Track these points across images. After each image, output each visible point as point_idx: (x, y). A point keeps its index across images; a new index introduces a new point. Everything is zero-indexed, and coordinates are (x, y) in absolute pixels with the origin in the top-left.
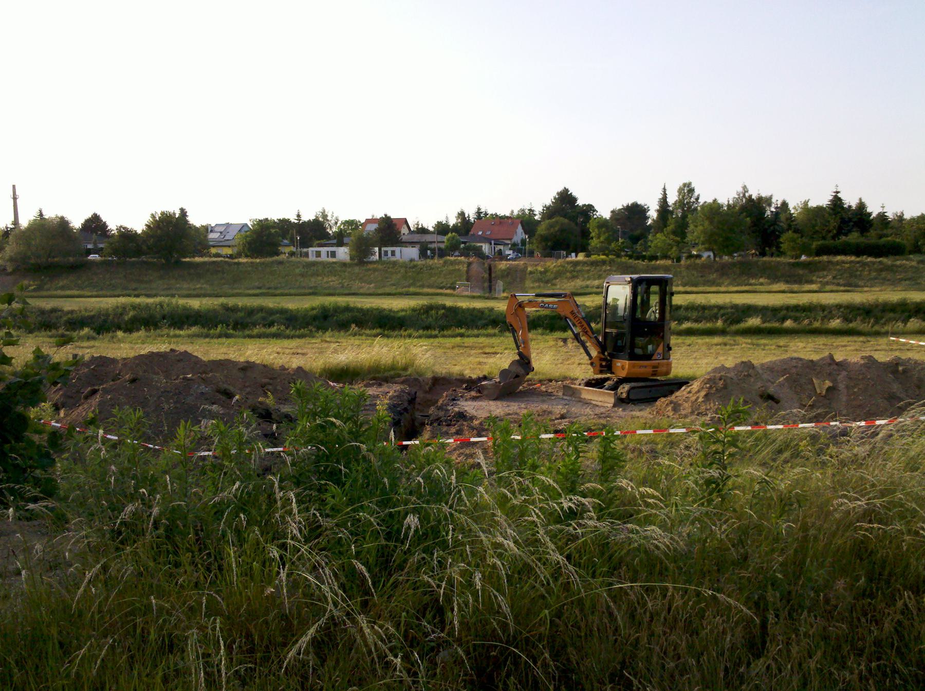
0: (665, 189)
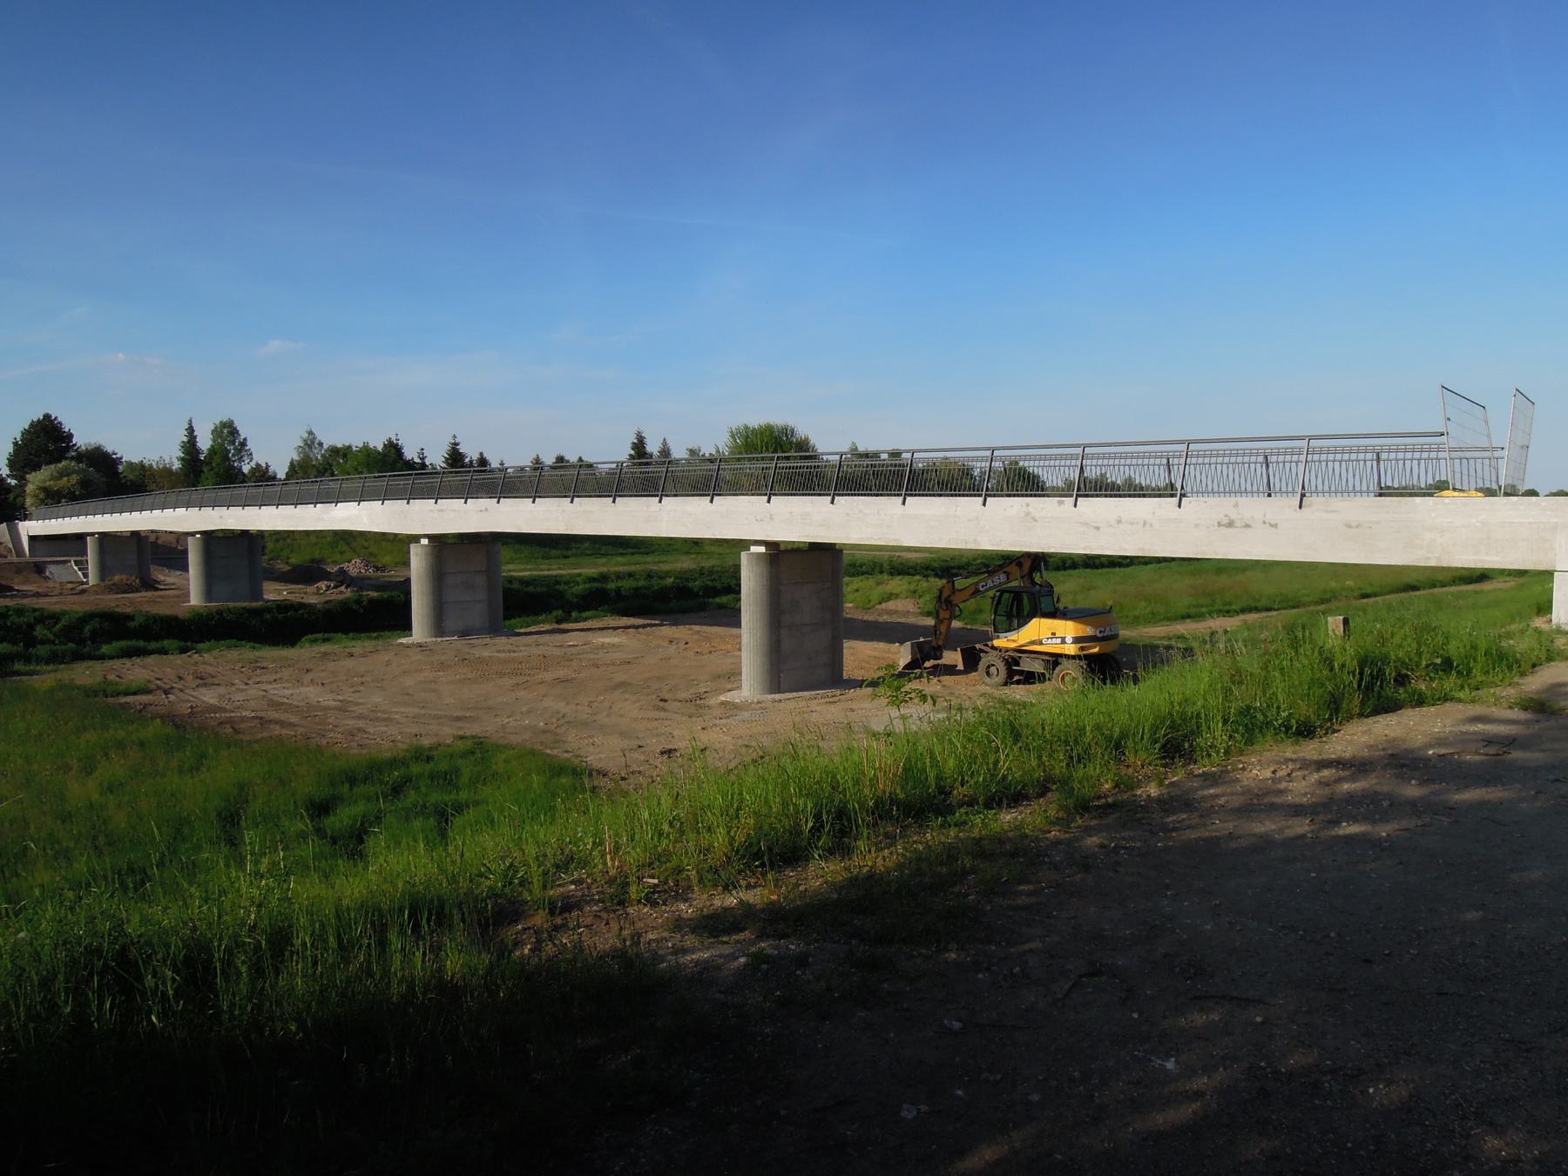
0: (191, 430)
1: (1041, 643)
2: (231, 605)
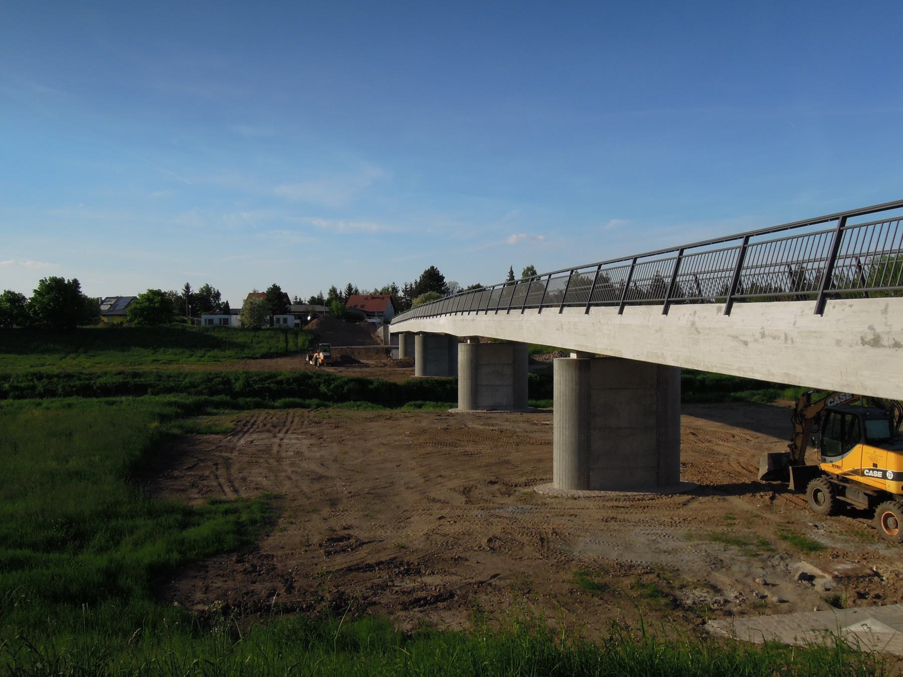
0: (512, 273)
1: (863, 475)
2: (436, 378)
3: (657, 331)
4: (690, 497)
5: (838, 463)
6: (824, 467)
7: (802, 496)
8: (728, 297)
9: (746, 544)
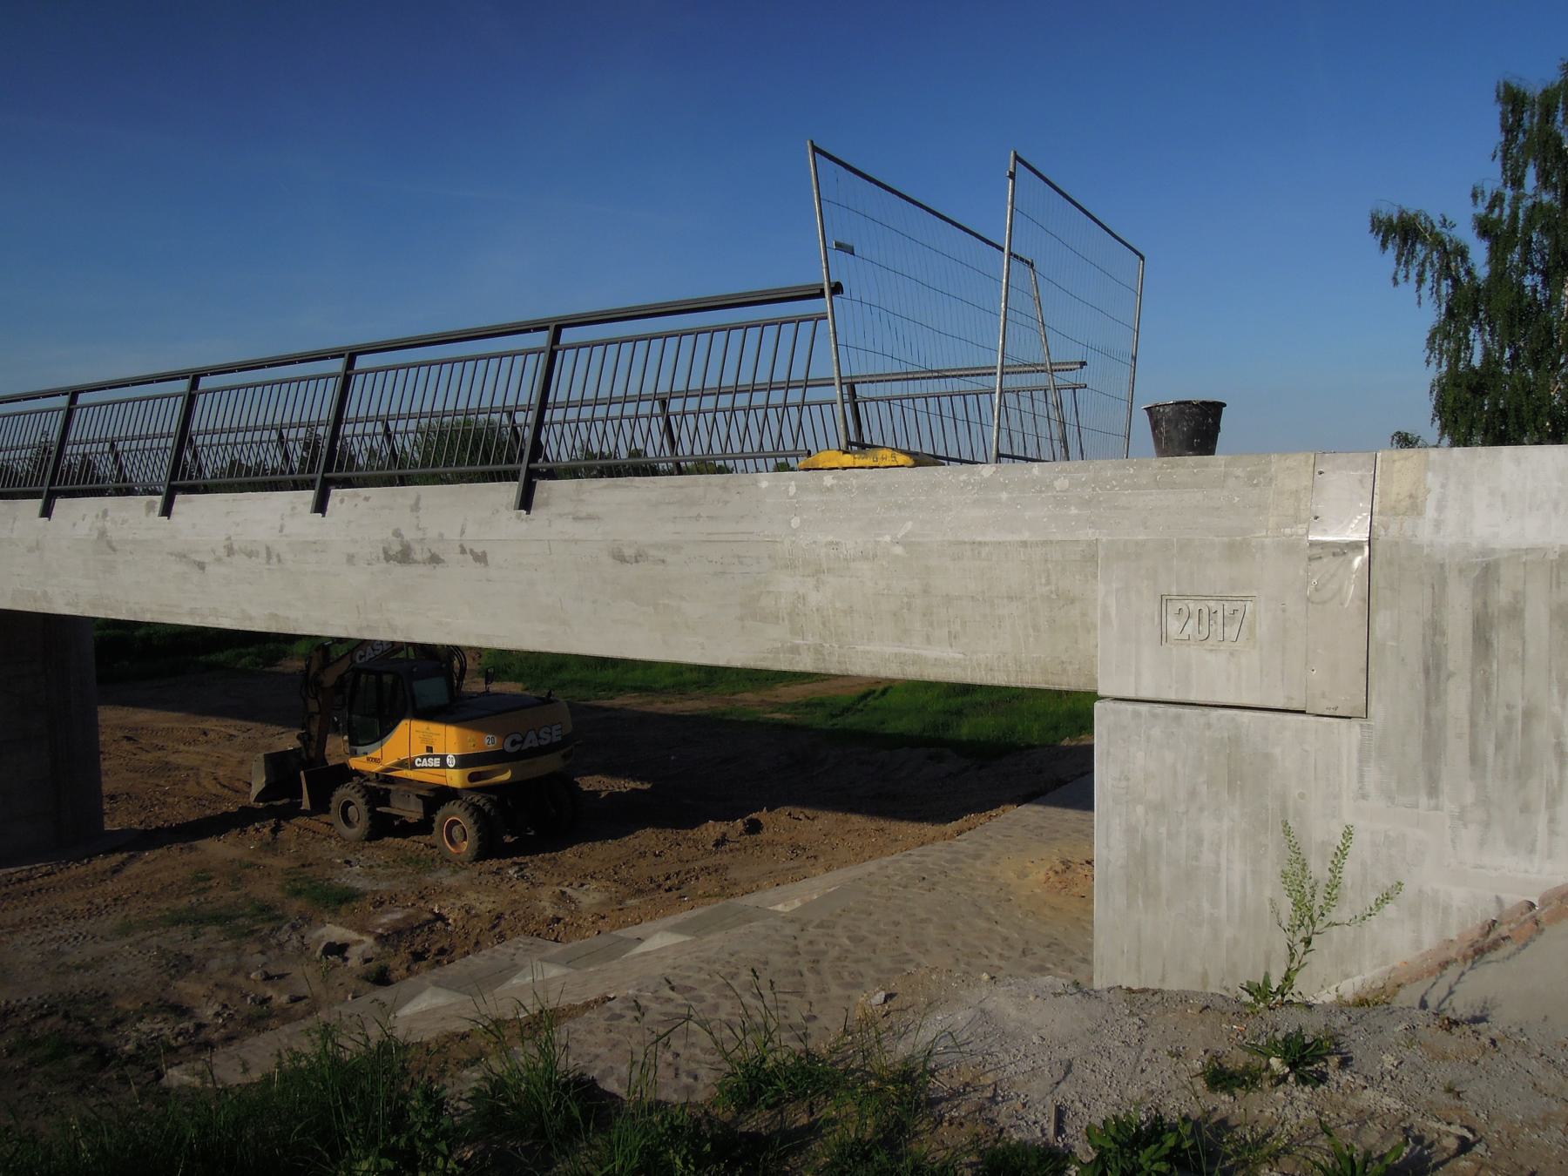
1: (413, 767)
3: (31, 550)
4: (125, 855)
5: (376, 754)
6: (356, 763)
7: (324, 818)
8: (523, 467)
9: (230, 918)
